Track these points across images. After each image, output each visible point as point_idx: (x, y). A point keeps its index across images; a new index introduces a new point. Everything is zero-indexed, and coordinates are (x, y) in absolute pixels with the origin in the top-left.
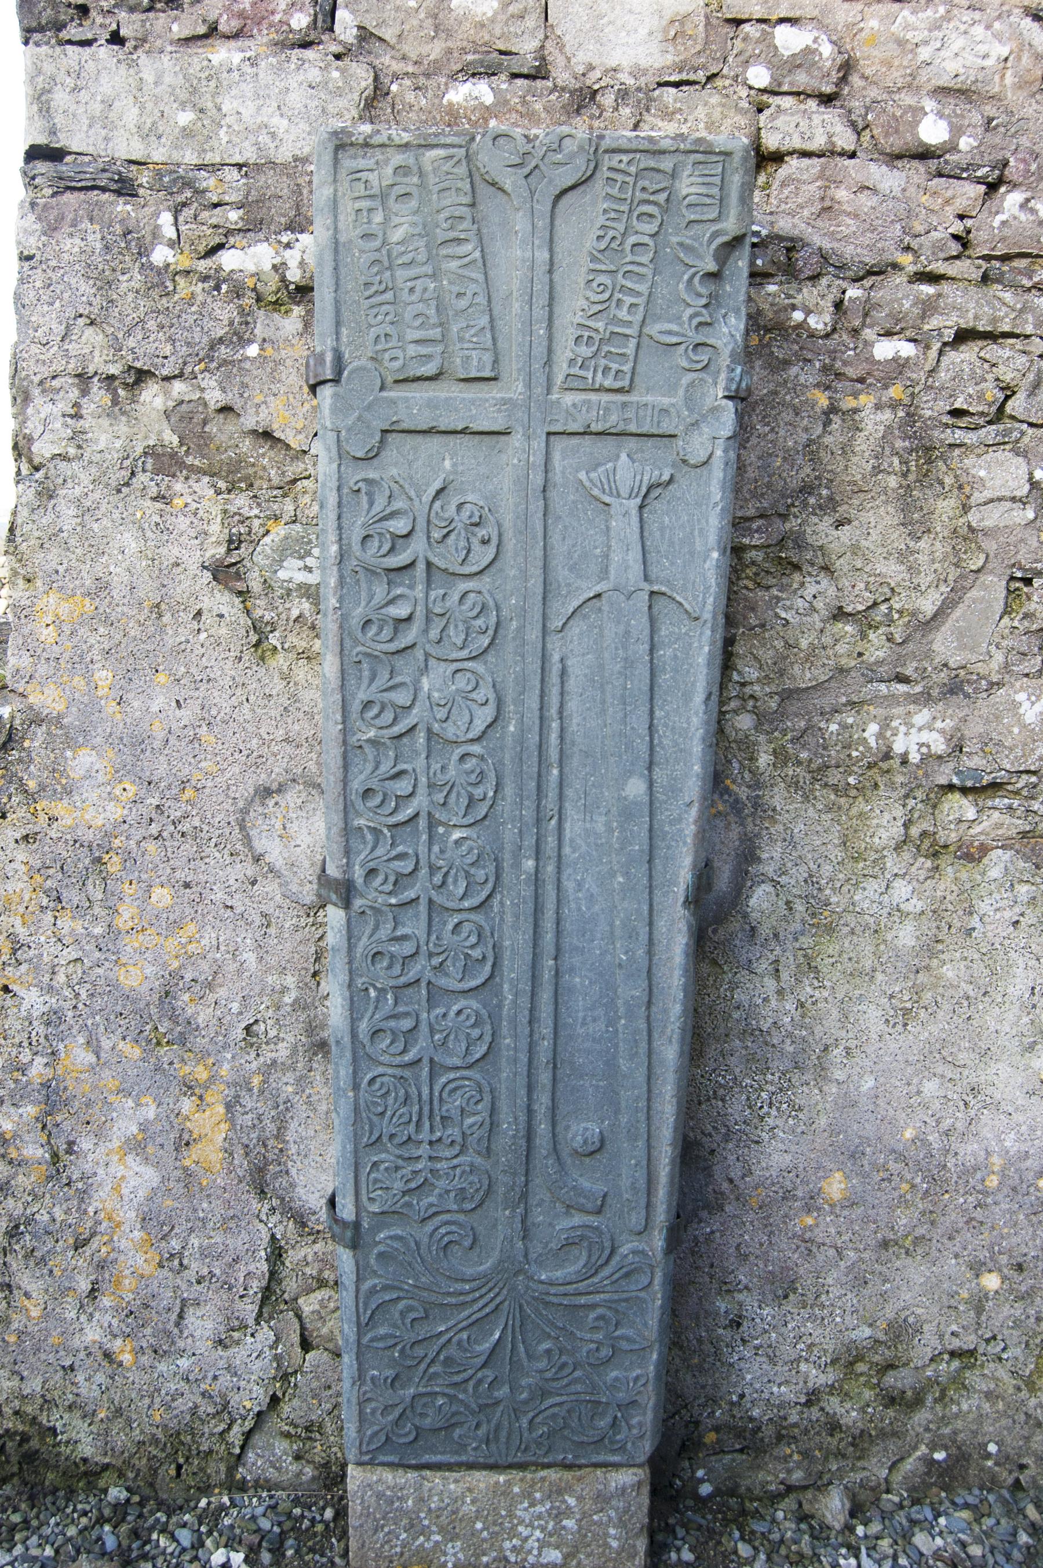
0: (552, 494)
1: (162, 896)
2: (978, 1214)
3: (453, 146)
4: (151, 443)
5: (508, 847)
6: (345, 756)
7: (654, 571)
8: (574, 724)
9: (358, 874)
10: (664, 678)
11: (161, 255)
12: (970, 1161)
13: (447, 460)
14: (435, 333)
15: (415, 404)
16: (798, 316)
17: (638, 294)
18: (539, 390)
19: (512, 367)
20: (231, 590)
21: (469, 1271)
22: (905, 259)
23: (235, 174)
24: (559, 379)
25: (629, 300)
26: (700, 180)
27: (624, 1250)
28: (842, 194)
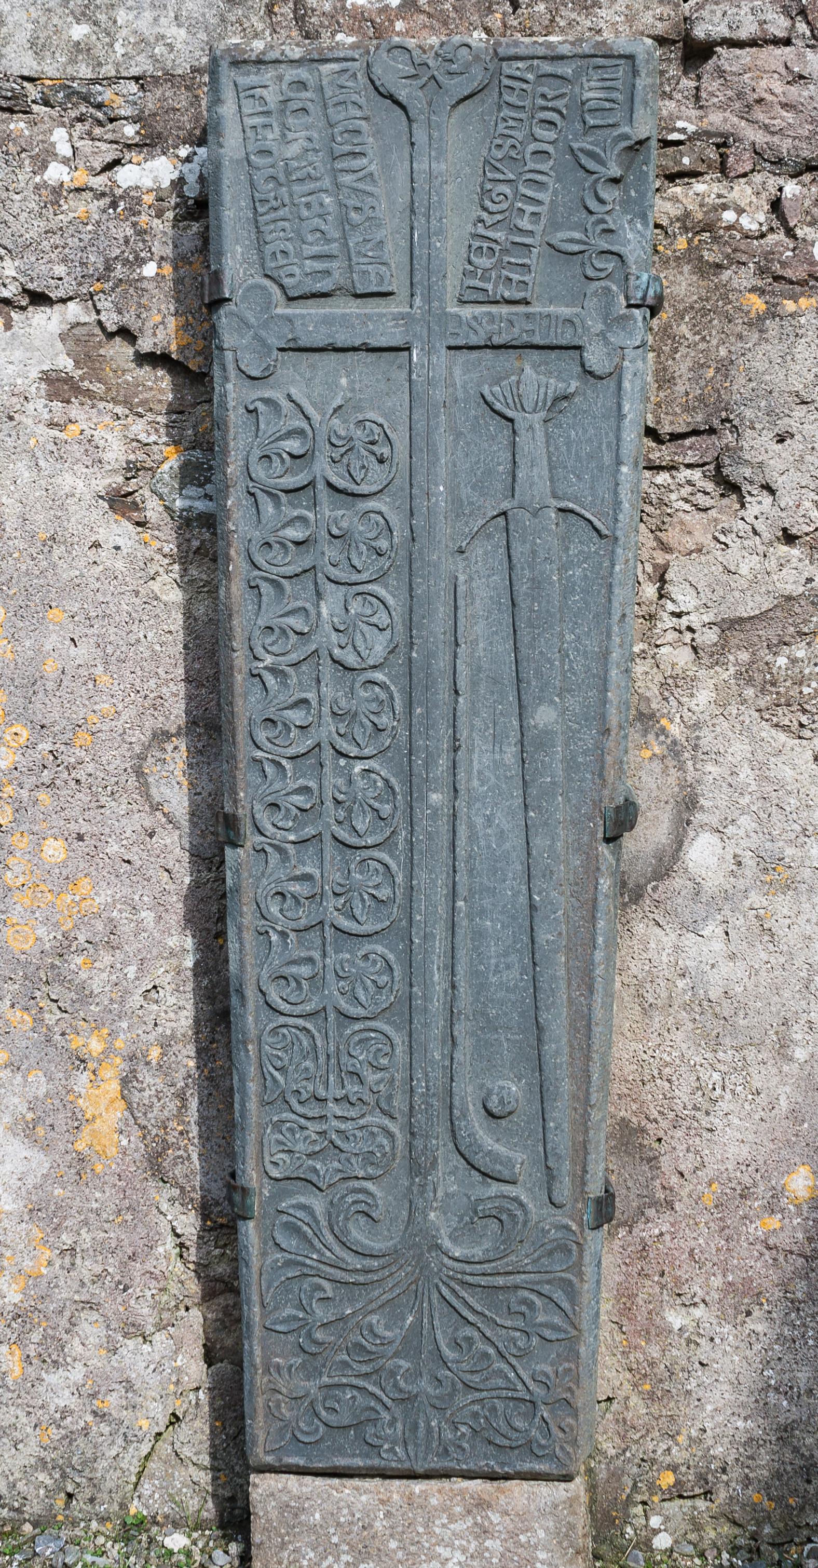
1: (54, 850)
3: (346, 60)
4: (46, 368)
11: (56, 173)
13: (346, 379)
15: (311, 321)
16: (729, 216)
17: (539, 202)
20: (129, 519)
25: (530, 209)
26: (600, 84)
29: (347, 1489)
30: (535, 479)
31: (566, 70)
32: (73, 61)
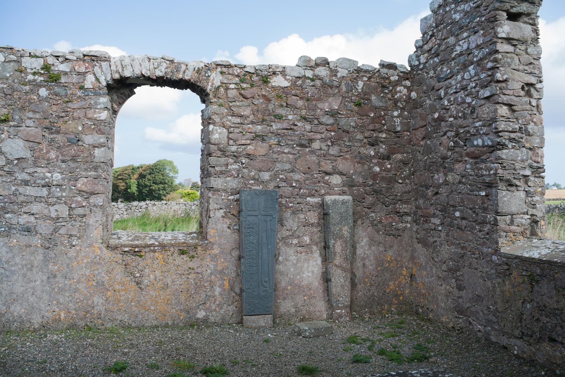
1: (222, 260)
11: (223, 197)
13: (253, 218)
29: (252, 317)
30: (269, 226)
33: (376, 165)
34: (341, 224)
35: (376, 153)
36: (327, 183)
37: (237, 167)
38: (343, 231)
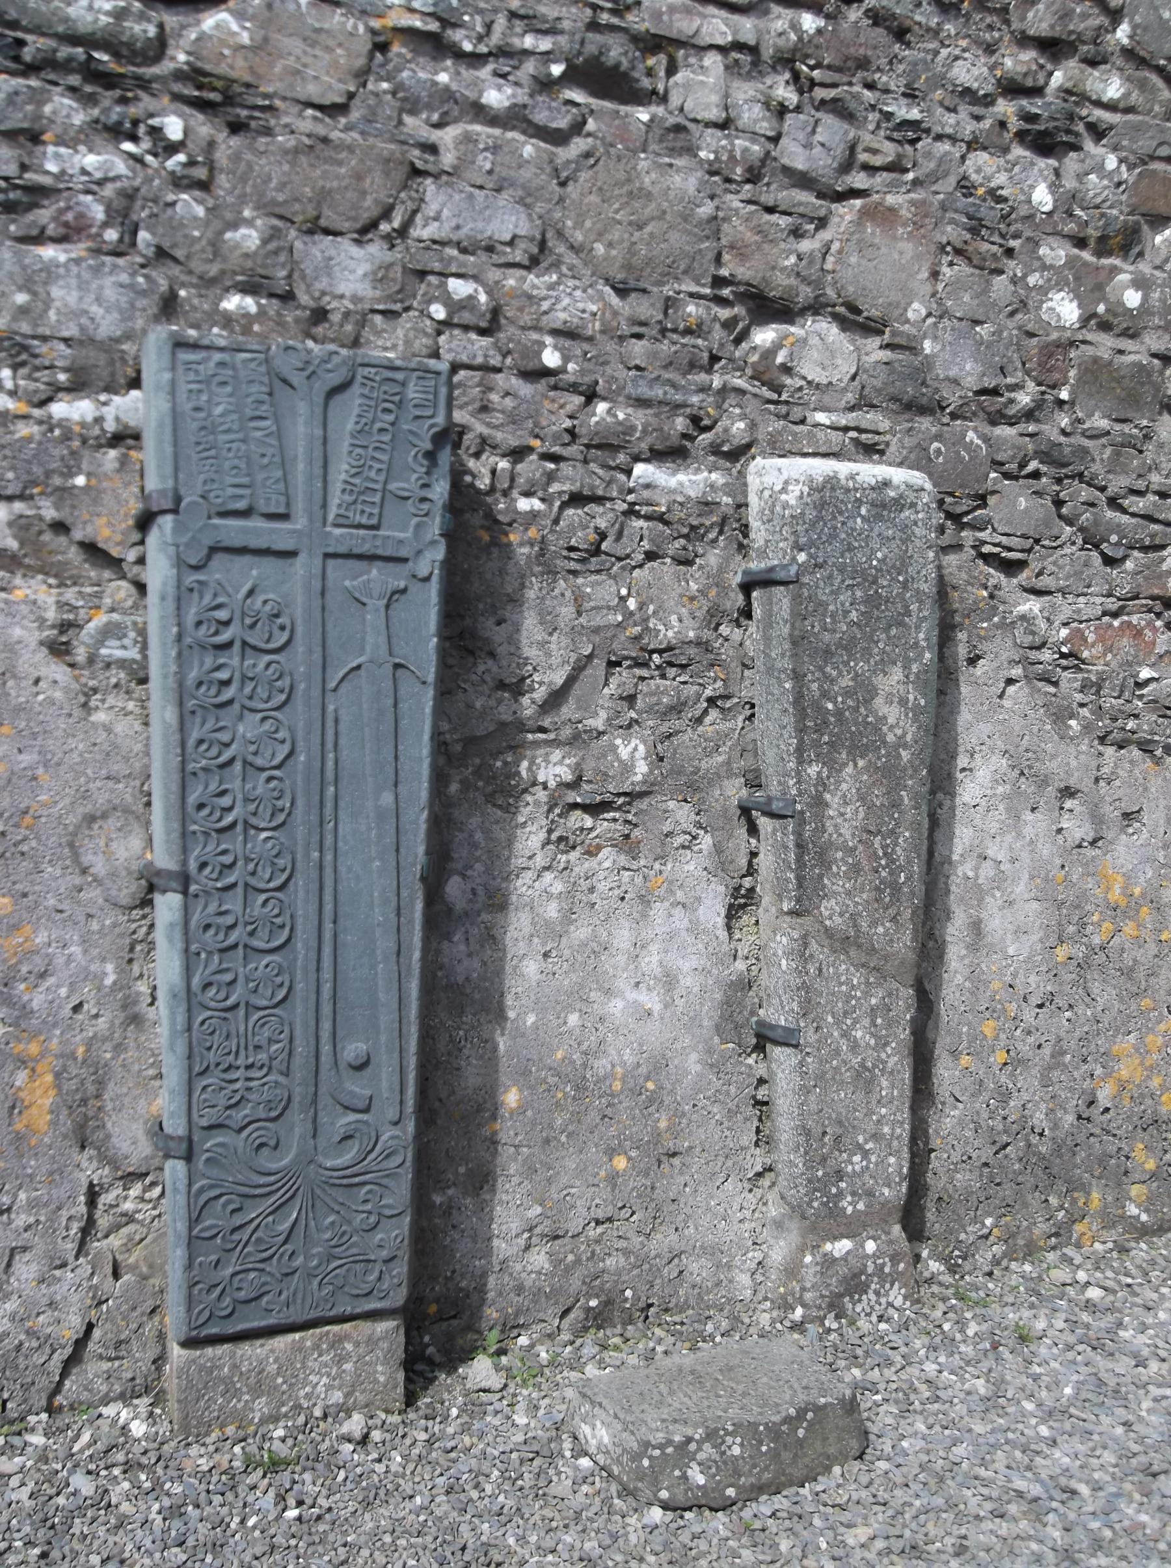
0: (328, 596)
2: (609, 1112)
5: (300, 842)
6: (183, 779)
7: (396, 650)
8: (344, 754)
9: (193, 866)
10: (404, 723)
12: (602, 1072)
13: (255, 570)
14: (245, 480)
16: (468, 478)
18: (318, 524)
19: (299, 507)
21: (274, 1166)
22: (536, 443)
23: (62, 346)
24: (331, 517)
25: (377, 466)
27: (383, 1138)
28: (494, 397)
31: (399, 376)
32: (15, 319)
33: (1058, 279)
34: (867, 654)
35: (1067, 203)
36: (770, 375)
37: (121, 167)
38: (879, 701)
